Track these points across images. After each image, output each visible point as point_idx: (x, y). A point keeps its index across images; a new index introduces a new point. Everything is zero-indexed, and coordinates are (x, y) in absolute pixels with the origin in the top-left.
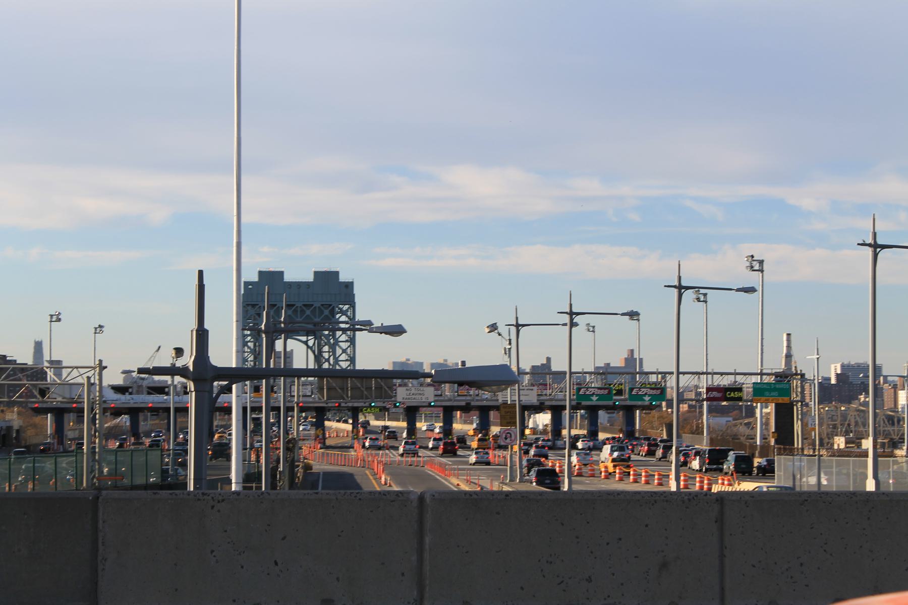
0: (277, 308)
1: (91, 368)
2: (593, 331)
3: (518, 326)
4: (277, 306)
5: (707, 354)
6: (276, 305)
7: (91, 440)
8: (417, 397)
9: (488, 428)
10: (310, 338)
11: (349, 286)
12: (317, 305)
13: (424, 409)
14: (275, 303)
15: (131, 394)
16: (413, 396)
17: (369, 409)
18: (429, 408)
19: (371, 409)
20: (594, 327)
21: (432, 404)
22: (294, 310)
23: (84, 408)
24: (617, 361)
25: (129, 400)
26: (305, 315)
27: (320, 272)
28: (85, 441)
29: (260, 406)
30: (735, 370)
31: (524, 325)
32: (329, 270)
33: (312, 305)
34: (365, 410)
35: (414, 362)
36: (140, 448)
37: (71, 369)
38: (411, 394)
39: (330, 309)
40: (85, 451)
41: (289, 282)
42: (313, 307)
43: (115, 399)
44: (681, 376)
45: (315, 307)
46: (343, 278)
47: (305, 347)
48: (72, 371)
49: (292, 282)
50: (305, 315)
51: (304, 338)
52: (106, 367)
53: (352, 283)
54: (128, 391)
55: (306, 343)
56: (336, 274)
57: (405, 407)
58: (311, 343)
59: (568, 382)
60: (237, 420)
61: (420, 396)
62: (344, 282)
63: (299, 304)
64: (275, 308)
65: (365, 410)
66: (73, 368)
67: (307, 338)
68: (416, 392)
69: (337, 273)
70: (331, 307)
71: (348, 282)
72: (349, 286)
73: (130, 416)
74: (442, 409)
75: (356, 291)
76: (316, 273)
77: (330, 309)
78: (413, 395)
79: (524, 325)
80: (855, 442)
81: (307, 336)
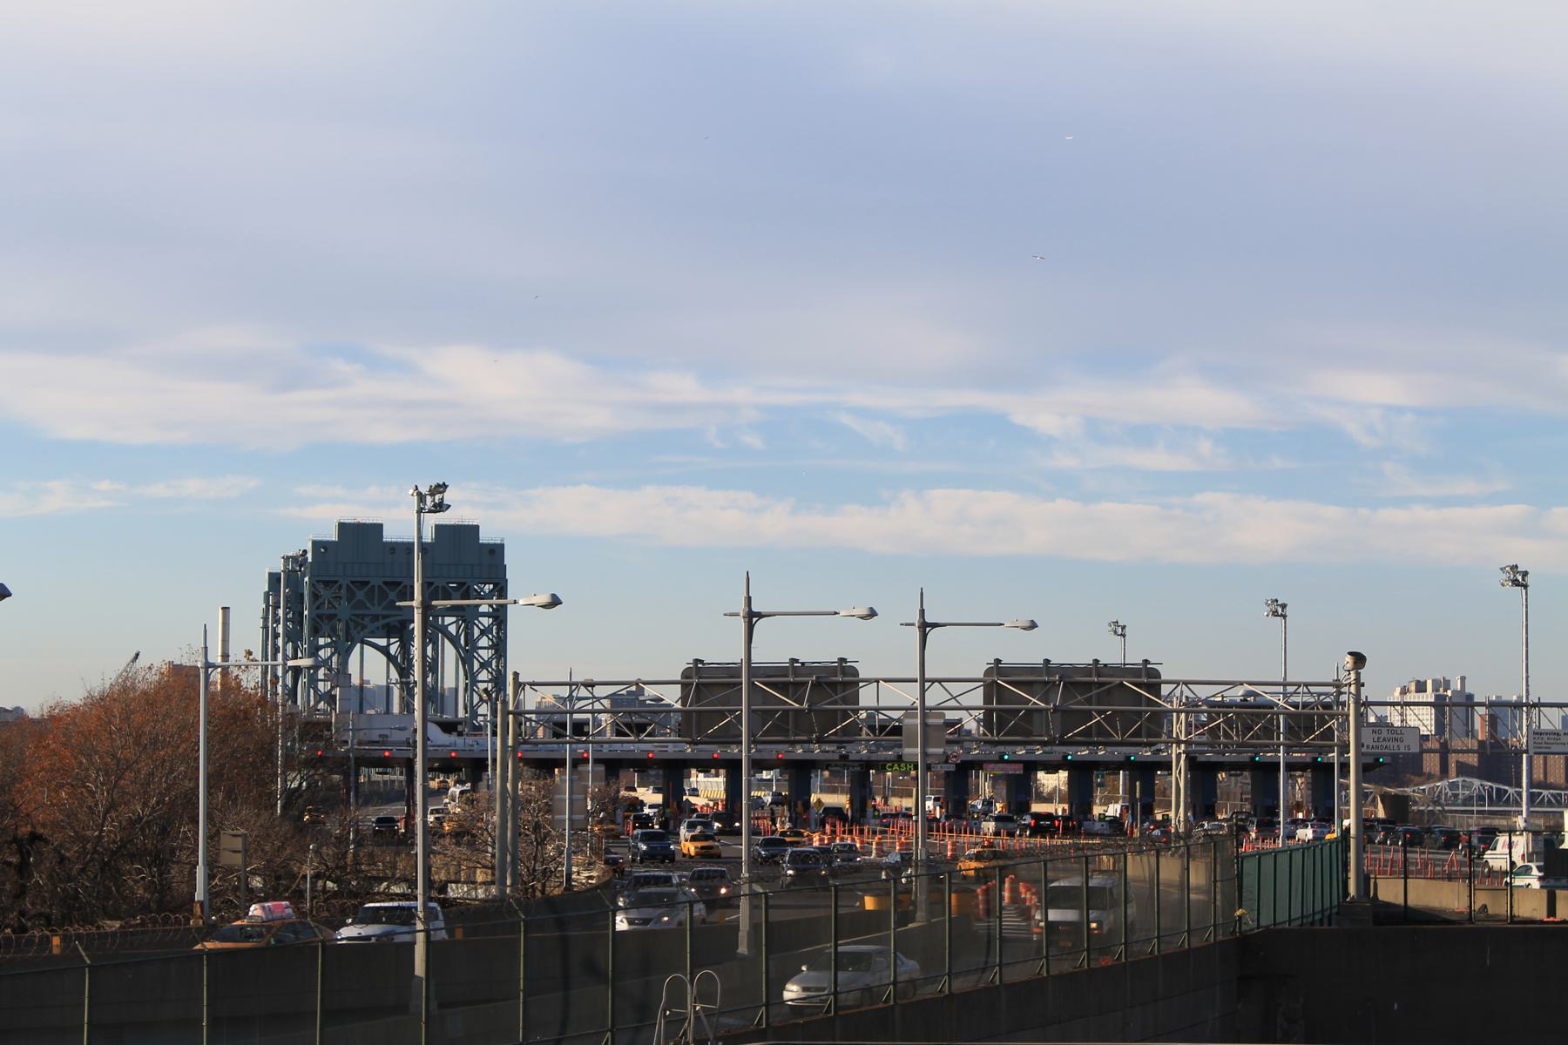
0: (371, 588)
2: (1123, 635)
3: (925, 627)
5: (1527, 677)
6: (367, 583)
7: (836, 812)
8: (1391, 744)
10: (392, 640)
11: (496, 551)
13: (991, 766)
14: (367, 579)
15: (460, 734)
16: (1384, 744)
17: (896, 765)
18: (1001, 765)
19: (899, 766)
20: (1124, 628)
21: (1006, 757)
23: (566, 759)
25: (472, 746)
26: (388, 600)
27: (446, 526)
31: (935, 625)
32: (460, 523)
33: (400, 583)
36: (1135, 830)
37: (1175, 685)
38: (1381, 740)
39: (462, 590)
42: (369, 586)
43: (447, 743)
45: (437, 587)
46: (485, 537)
47: (384, 659)
48: (1176, 688)
50: (388, 600)
51: (382, 642)
52: (1363, 685)
53: (502, 546)
54: (456, 730)
56: (378, 528)
57: (959, 762)
58: (393, 649)
59: (1524, 721)
61: (1396, 744)
62: (488, 545)
63: (376, 582)
66: (1177, 683)
67: (388, 641)
68: (1390, 736)
69: (476, 528)
70: (465, 588)
71: (495, 545)
72: (496, 551)
73: (726, 772)
74: (1021, 765)
75: (509, 559)
76: (343, 527)
77: (462, 590)
78: (1384, 740)
79: (935, 625)
80: (638, 828)
81: (389, 637)
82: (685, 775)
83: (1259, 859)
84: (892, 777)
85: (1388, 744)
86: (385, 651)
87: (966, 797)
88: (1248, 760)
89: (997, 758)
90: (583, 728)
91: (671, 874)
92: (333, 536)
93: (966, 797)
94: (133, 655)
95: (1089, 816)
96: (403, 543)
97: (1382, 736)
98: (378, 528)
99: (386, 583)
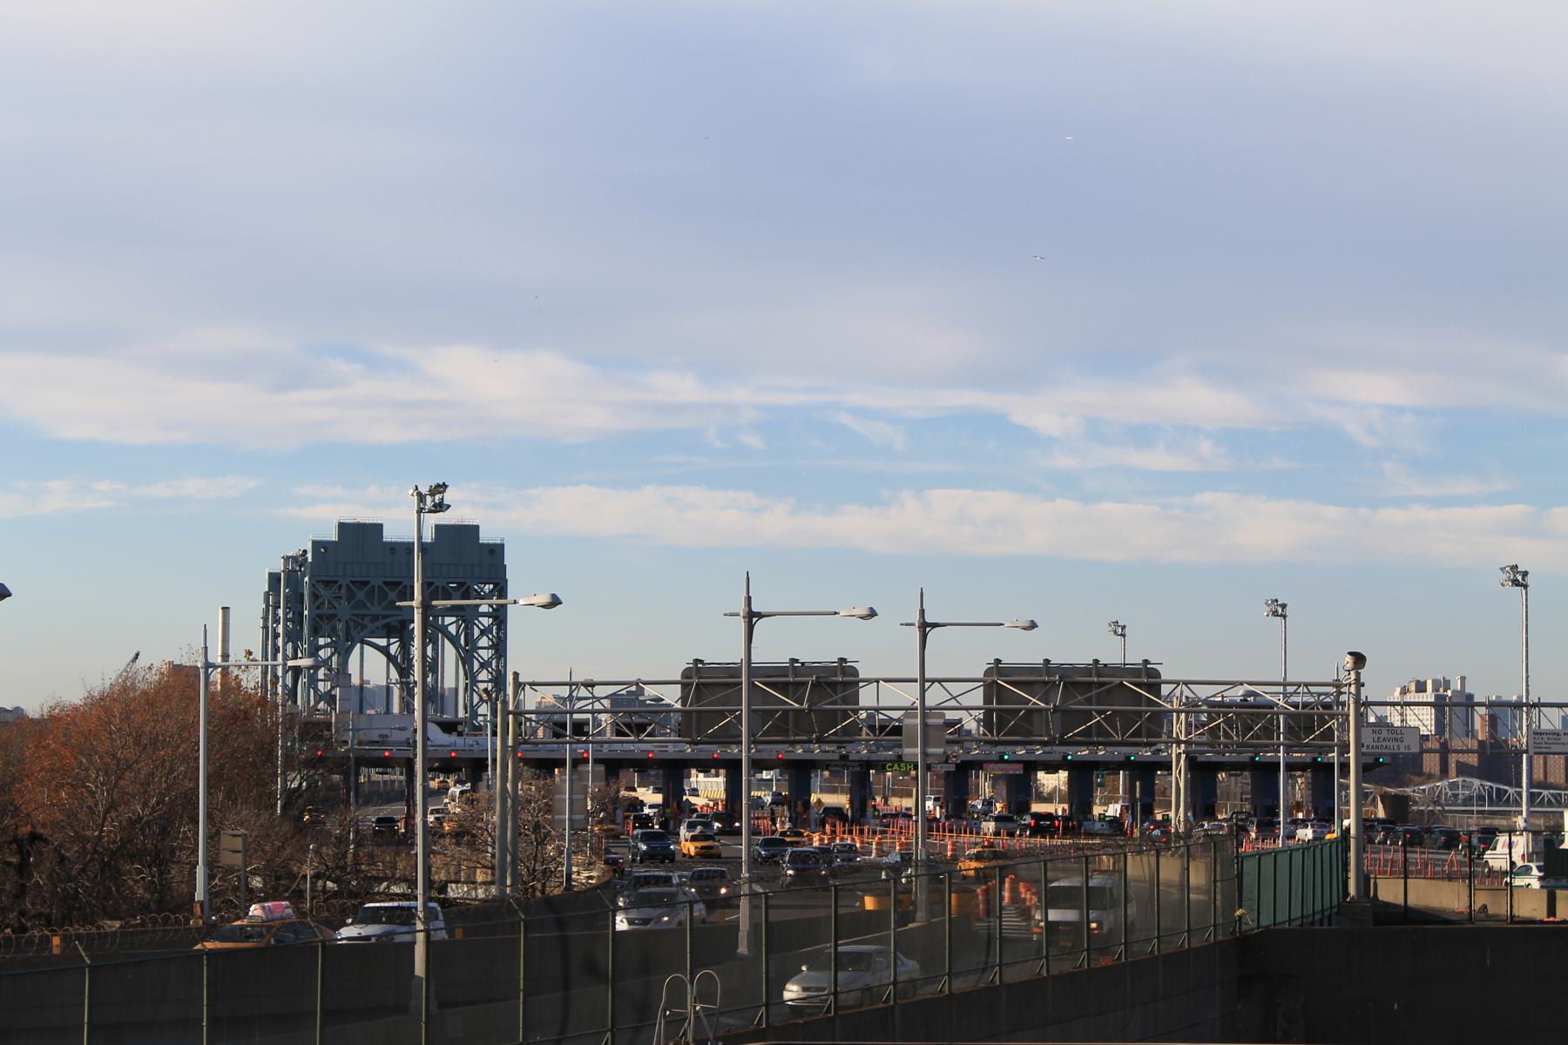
1: (1230, 684)
2: (1123, 635)
3: (925, 627)
4: (370, 585)
5: (1527, 677)
6: (368, 583)
7: (836, 812)
8: (1391, 744)
9: (966, 797)
10: (392, 640)
11: (496, 551)
13: (991, 766)
15: (460, 734)
16: (1384, 744)
19: (899, 766)
20: (1124, 628)
21: (1006, 757)
22: (400, 591)
23: (566, 759)
24: (87, 694)
25: (472, 746)
26: (388, 600)
27: (446, 526)
28: (1281, 819)
29: (483, 756)
30: (1539, 698)
31: (935, 625)
32: (460, 523)
33: (400, 583)
34: (890, 767)
35: (378, 686)
36: (1135, 830)
37: (1175, 685)
38: (1381, 740)
39: (461, 591)
41: (391, 543)
44: (1464, 708)
46: (485, 537)
47: (384, 659)
48: (1176, 688)
49: (396, 543)
50: (388, 600)
51: (382, 642)
53: (502, 546)
54: (456, 730)
55: (385, 651)
56: (378, 528)
57: (959, 762)
58: (393, 649)
59: (1524, 721)
60: (1124, 784)
61: (1396, 744)
62: (488, 545)
63: (376, 581)
64: (368, 587)
65: (890, 767)
66: (1177, 683)
67: (388, 641)
72: (496, 551)
74: (1022, 765)
75: (509, 559)
76: (342, 527)
78: (1384, 740)
79: (935, 625)
81: (389, 637)
83: (1275, 855)
84: (892, 777)
85: (1388, 743)
88: (1248, 760)
93: (966, 797)
94: (133, 655)
95: (1089, 816)
96: (403, 543)
97: (1382, 736)
99: (386, 583)
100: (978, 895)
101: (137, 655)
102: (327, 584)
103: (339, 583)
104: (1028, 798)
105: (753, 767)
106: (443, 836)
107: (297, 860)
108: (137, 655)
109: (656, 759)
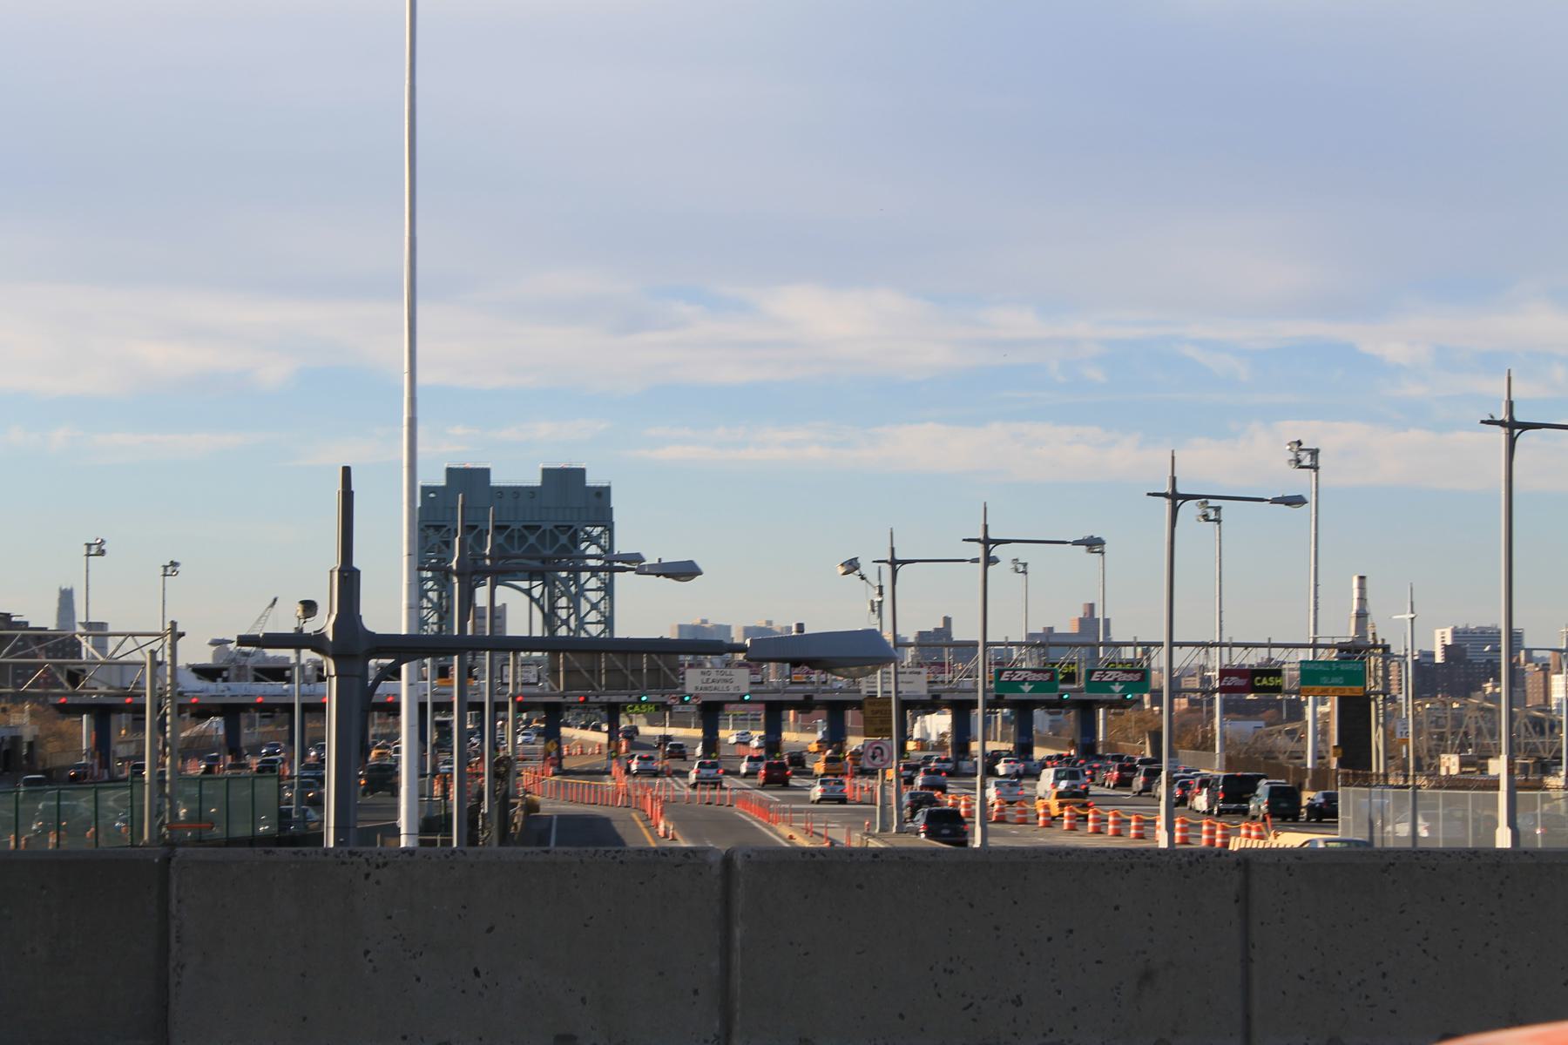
0: (479, 532)
2: (1025, 572)
3: (894, 563)
4: (479, 529)
8: (720, 685)
10: (535, 583)
11: (603, 494)
12: (548, 526)
13: (733, 706)
14: (476, 524)
15: (226, 680)
16: (713, 685)
17: (637, 707)
18: (741, 706)
19: (640, 707)
20: (1025, 565)
21: (747, 698)
23: (145, 705)
24: (1066, 624)
25: (223, 691)
26: (527, 544)
29: (449, 701)
30: (1270, 639)
31: (904, 562)
33: (540, 527)
37: (123, 638)
38: (710, 681)
39: (569, 533)
40: (147, 778)
41: (499, 487)
44: (1176, 649)
46: (592, 480)
47: (527, 599)
49: (504, 488)
50: (527, 544)
51: (525, 585)
53: (608, 489)
54: (220, 676)
57: (700, 702)
58: (536, 593)
61: (726, 685)
62: (594, 488)
63: (516, 526)
64: (557, 532)
65: (631, 708)
66: (126, 635)
67: (531, 584)
68: (719, 677)
70: (572, 530)
72: (603, 494)
74: (763, 706)
75: (616, 502)
77: (569, 533)
78: (713, 681)
79: (904, 562)
81: (531, 580)
82: (784, 717)
83: (253, 780)
84: (261, 712)
85: (717, 685)
86: (528, 592)
87: (968, 738)
88: (1057, 698)
89: (738, 699)
90: (284, 674)
91: (75, 803)
92: (536, 480)
93: (968, 738)
94: (271, 601)
95: (1485, 772)
96: (527, 487)
97: (712, 677)
98: (581, 473)
99: (526, 527)
100: (165, 811)
101: (275, 600)
102: (438, 528)
103: (479, 529)
104: (706, 737)
105: (1224, 713)
106: (1382, 803)
107: (1383, 833)
108: (275, 600)
109: (1073, 700)
